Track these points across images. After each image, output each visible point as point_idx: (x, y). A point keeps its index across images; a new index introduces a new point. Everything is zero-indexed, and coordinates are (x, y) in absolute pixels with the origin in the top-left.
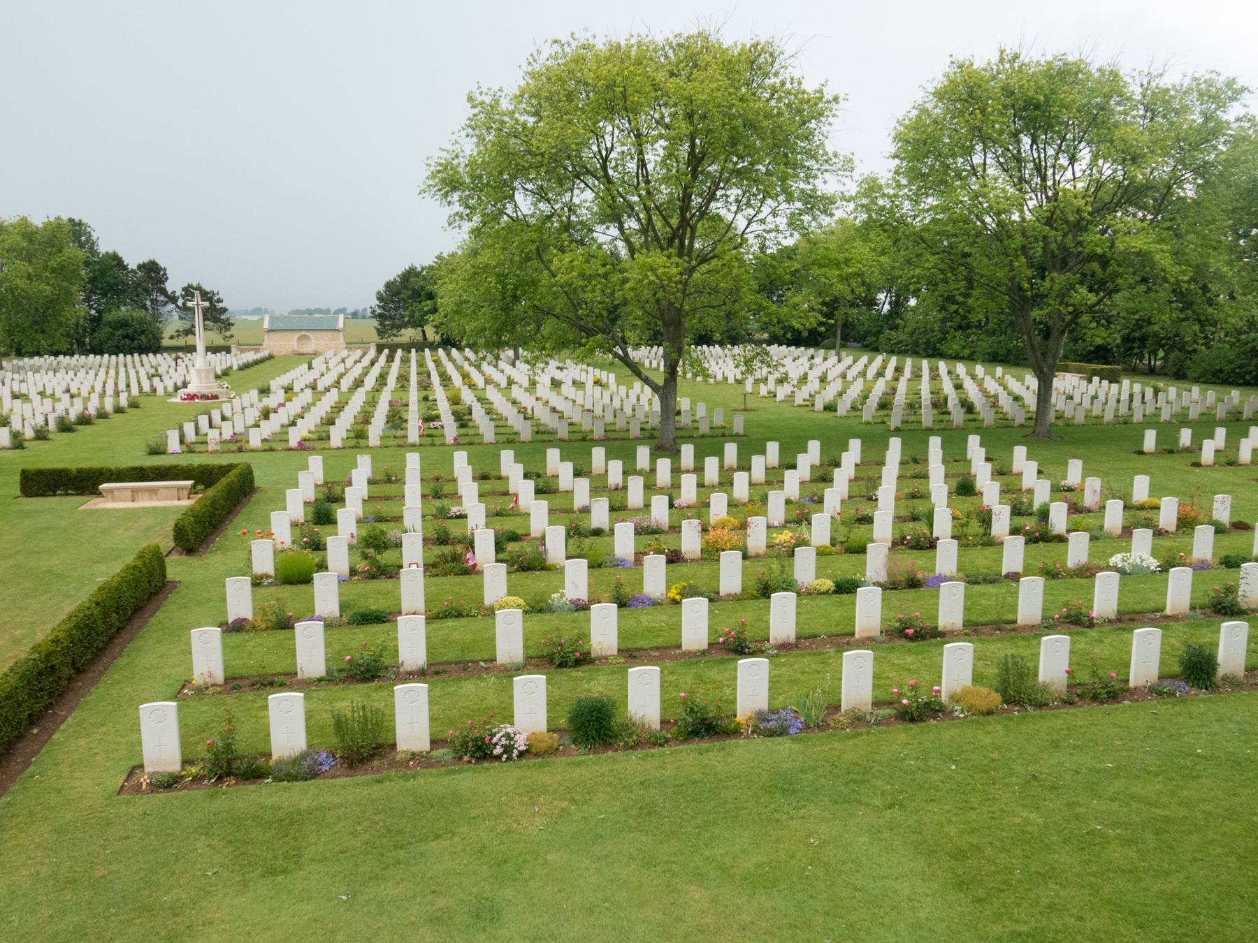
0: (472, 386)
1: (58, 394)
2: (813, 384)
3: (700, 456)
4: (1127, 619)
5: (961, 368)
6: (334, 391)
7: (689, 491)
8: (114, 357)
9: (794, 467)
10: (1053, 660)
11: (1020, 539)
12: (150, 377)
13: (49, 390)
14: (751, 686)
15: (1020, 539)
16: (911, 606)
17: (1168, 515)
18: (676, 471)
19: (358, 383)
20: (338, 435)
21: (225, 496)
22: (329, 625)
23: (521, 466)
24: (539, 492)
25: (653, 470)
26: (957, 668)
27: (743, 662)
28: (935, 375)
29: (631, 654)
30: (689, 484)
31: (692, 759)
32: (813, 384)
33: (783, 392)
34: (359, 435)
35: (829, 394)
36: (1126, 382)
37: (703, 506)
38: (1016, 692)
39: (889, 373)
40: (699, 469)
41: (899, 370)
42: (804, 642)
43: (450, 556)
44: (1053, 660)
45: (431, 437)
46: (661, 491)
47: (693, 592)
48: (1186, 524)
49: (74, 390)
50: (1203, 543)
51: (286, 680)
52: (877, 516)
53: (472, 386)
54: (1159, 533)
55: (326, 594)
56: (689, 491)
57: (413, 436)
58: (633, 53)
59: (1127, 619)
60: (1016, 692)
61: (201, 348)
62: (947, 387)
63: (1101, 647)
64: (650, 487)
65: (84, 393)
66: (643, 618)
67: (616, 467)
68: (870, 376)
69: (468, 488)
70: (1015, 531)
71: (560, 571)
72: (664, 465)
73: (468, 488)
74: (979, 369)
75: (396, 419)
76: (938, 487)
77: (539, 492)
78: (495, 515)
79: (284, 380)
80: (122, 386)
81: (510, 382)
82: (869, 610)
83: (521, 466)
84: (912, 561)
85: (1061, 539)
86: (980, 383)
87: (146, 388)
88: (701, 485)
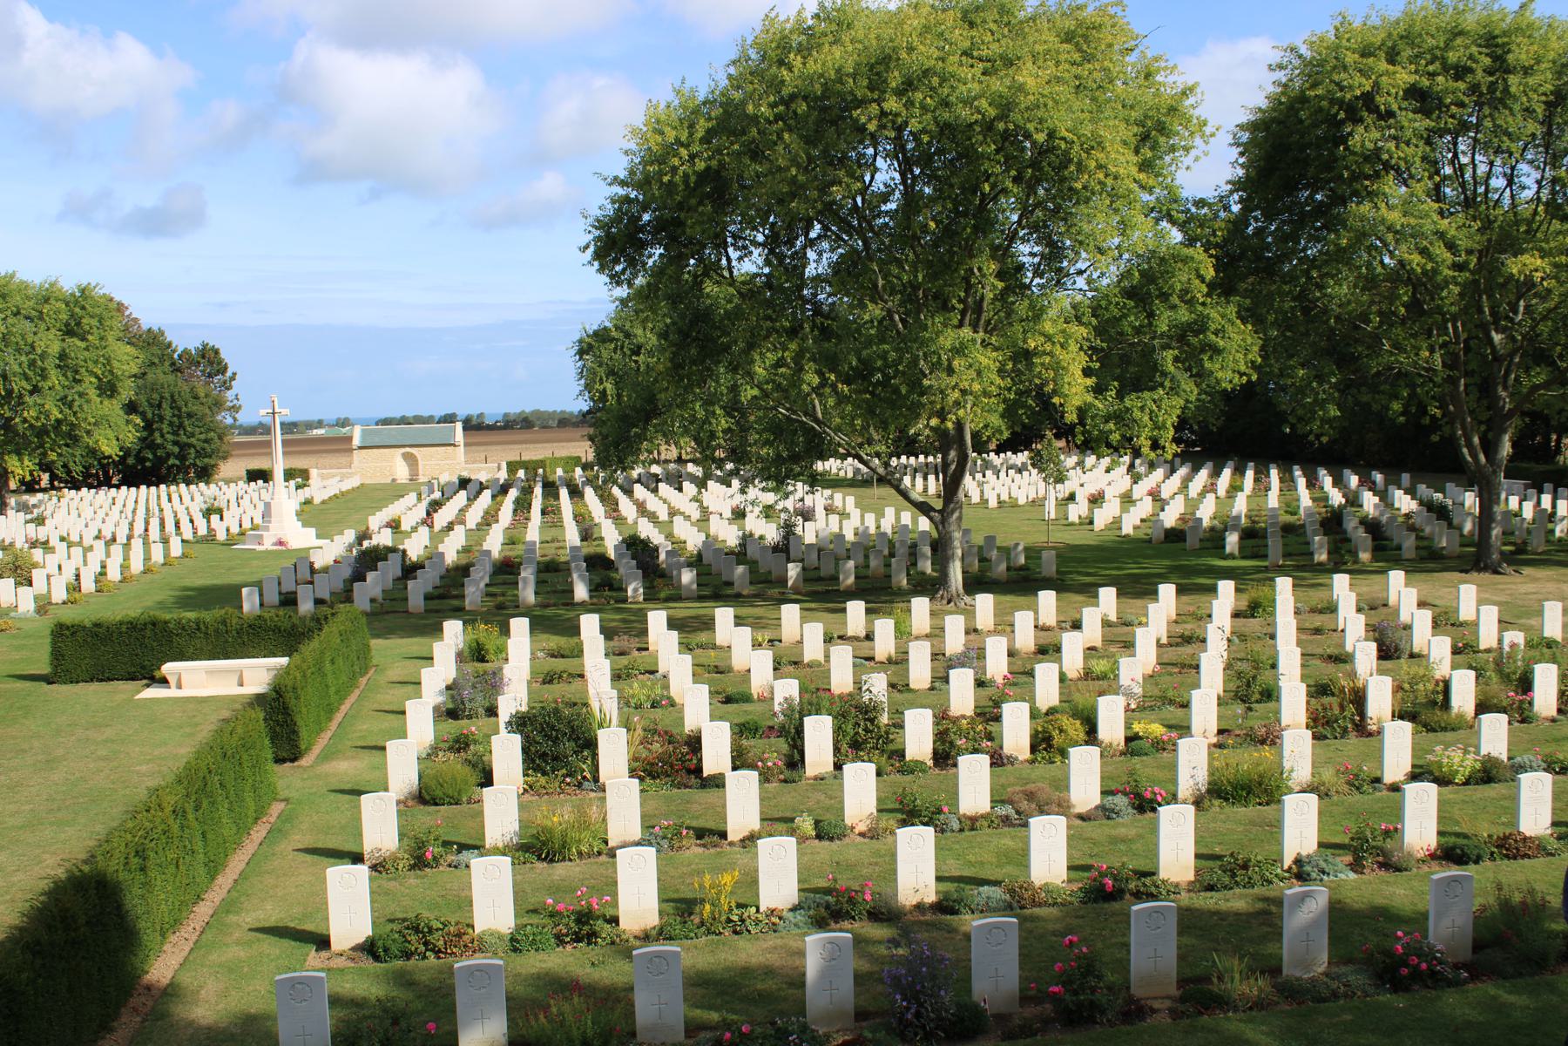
0: (652, 517)
1: (87, 542)
6: (459, 529)
8: (153, 489)
9: (1077, 626)
12: (208, 513)
13: (95, 541)
18: (903, 634)
22: (1198, 803)
23: (1414, 591)
25: (869, 637)
33: (1102, 517)
40: (937, 634)
43: (1338, 713)
46: (961, 661)
47: (910, 815)
49: (75, 538)
53: (652, 517)
55: (502, 810)
58: (1508, 20)
61: (279, 474)
64: (865, 660)
65: (122, 539)
68: (1222, 492)
71: (718, 782)
72: (885, 628)
80: (170, 526)
81: (673, 513)
83: (1414, 591)
85: (718, 782)
87: (202, 531)
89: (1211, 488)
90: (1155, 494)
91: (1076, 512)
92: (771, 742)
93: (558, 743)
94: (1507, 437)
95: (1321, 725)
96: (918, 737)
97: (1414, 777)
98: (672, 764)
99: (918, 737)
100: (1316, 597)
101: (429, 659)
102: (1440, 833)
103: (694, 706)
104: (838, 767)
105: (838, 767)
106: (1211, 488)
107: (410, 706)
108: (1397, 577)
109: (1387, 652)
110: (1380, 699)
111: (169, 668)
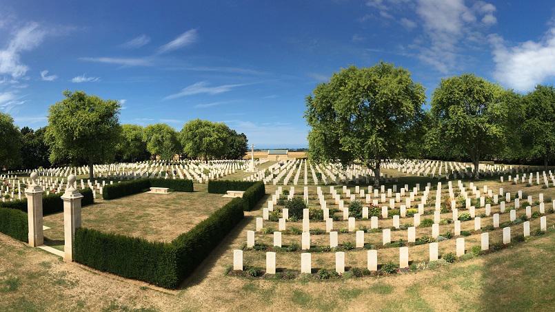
2: (417, 169)
3: (386, 190)
4: (502, 226)
5: (455, 163)
7: (383, 199)
10: (340, 261)
11: (474, 207)
14: (404, 256)
15: (474, 207)
16: (288, 261)
17: (508, 197)
19: (291, 168)
20: (286, 181)
21: (257, 195)
24: (342, 198)
26: (433, 251)
27: (369, 251)
28: (448, 165)
29: (367, 246)
30: (383, 196)
31: (353, 283)
32: (417, 169)
33: (408, 171)
34: (291, 181)
35: (421, 171)
36: (495, 165)
37: (387, 202)
38: (322, 273)
39: (437, 165)
41: (439, 165)
42: (418, 242)
44: (340, 261)
45: (311, 183)
48: (512, 199)
50: (517, 203)
51: (528, 204)
52: (436, 204)
54: (506, 203)
56: (383, 199)
57: (306, 183)
59: (502, 226)
60: (322, 273)
62: (452, 168)
63: (389, 253)
66: (220, 268)
67: (362, 191)
69: (321, 197)
70: (472, 205)
73: (321, 197)
74: (460, 164)
75: (302, 177)
76: (452, 194)
77: (342, 198)
78: (329, 204)
79: (272, 167)
82: (436, 231)
84: (447, 216)
86: (460, 167)
88: (386, 197)
89: (435, 165)
90: (419, 167)
91: (404, 170)
92: (355, 210)
93: (446, 208)
94: (83, 79)
95: (443, 212)
96: (385, 212)
97: (333, 230)
98: (316, 216)
99: (385, 212)
100: (445, 186)
101: (423, 195)
102: (300, 259)
103: (340, 204)
104: (370, 217)
105: (370, 217)
106: (435, 165)
107: (419, 205)
108: (460, 181)
109: (456, 195)
110: (453, 204)
111: (228, 192)
